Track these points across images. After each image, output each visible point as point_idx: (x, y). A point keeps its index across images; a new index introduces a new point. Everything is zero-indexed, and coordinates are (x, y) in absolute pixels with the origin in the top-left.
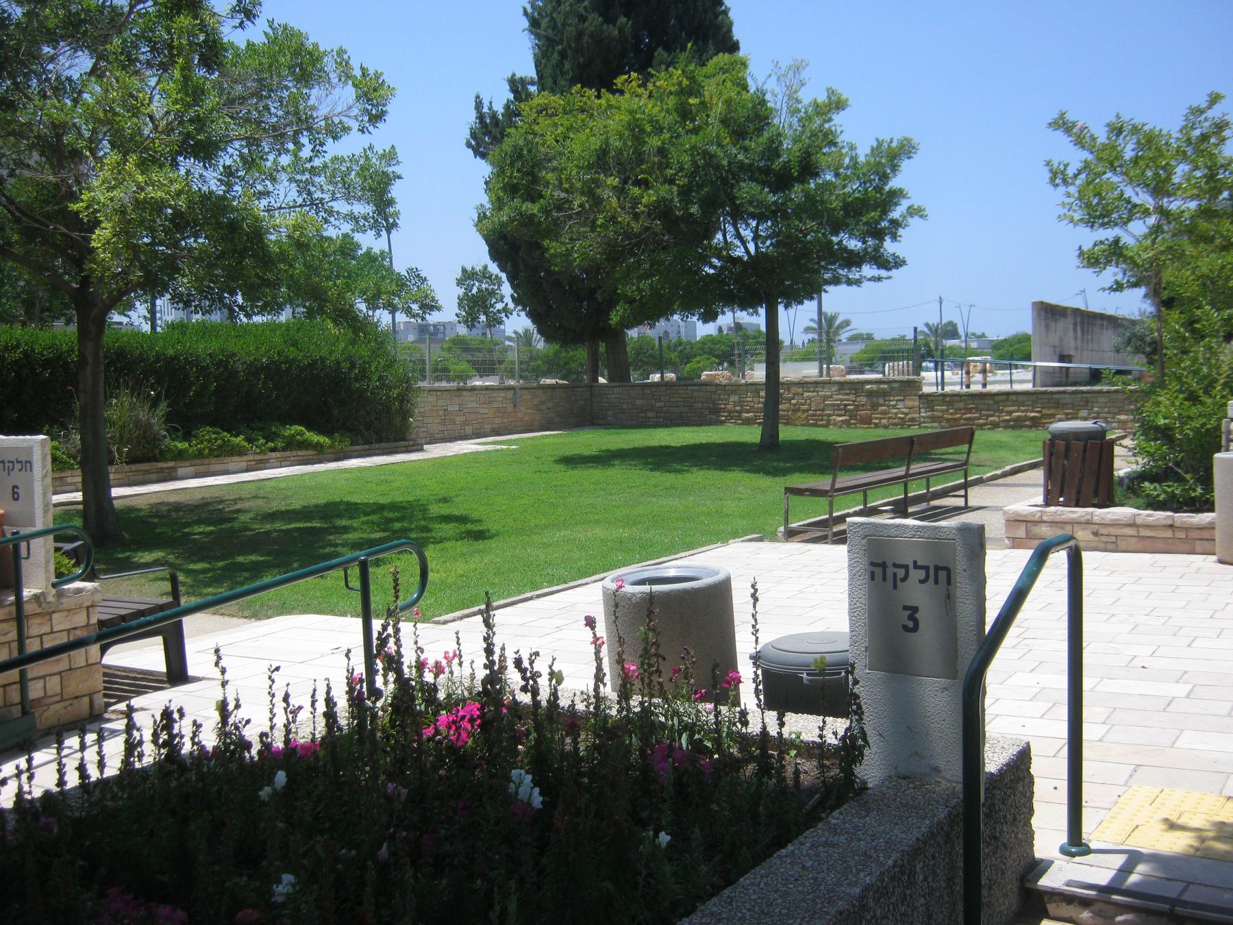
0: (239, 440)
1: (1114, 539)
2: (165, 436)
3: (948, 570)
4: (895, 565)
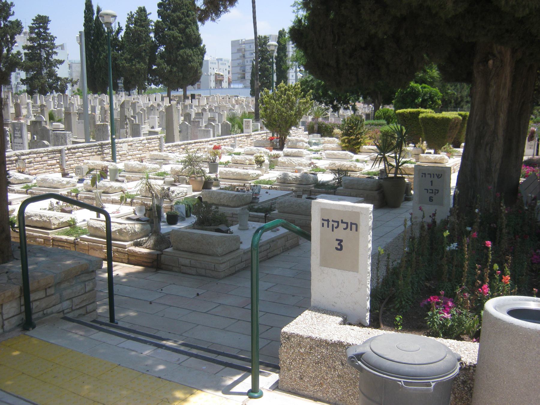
0: (137, 166)
1: (234, 216)
2: (508, 274)
3: (356, 225)
4: (333, 221)
